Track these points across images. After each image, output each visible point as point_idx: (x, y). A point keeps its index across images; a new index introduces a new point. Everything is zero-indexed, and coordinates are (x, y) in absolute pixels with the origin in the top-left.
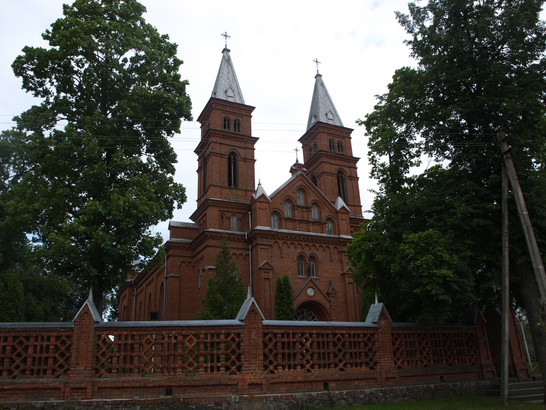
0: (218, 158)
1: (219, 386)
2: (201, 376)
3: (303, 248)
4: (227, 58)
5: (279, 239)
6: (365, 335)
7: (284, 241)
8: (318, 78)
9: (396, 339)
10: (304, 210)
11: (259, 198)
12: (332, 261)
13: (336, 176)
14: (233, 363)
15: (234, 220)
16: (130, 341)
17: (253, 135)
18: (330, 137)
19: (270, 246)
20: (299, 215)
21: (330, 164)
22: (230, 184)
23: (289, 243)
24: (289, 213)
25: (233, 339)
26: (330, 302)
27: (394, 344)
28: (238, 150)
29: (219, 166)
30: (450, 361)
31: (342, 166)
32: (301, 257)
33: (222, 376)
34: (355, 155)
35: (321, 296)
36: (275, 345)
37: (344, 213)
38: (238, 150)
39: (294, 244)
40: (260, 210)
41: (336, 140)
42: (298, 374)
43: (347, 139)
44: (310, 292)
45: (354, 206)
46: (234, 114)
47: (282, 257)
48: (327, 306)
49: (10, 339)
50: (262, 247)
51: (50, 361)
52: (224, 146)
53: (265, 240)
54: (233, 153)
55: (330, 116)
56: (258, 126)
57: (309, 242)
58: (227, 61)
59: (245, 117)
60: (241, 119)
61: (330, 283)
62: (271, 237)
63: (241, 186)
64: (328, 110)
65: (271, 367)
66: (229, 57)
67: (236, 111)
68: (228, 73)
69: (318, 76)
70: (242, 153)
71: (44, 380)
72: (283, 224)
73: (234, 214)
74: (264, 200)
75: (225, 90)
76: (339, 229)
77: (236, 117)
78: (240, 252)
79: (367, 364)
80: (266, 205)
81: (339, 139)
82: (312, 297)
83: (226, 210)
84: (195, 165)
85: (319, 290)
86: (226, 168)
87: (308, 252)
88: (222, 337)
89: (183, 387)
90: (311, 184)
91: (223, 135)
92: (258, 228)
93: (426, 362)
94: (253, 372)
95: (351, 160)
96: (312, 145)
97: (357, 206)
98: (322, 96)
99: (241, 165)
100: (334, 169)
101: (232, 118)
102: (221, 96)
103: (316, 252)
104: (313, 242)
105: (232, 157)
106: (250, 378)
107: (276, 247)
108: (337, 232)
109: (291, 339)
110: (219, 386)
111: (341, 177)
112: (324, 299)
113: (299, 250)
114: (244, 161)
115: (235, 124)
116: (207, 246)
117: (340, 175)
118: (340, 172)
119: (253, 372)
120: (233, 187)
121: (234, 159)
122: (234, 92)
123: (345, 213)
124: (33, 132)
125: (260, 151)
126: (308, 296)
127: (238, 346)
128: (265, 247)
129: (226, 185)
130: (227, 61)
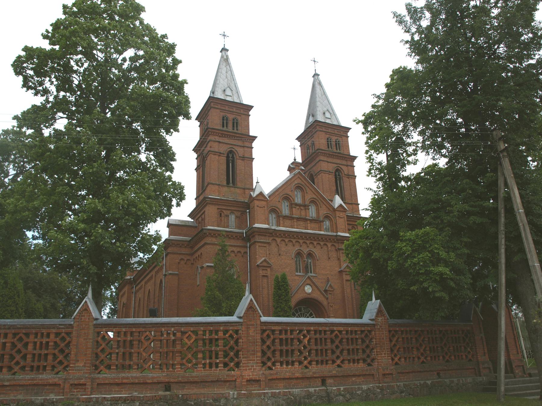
0: (217, 157)
1: (217, 382)
2: (200, 373)
3: (301, 246)
4: (225, 57)
5: (277, 237)
6: (362, 332)
7: (282, 239)
8: (316, 77)
9: (393, 336)
10: (302, 208)
11: (258, 196)
12: (329, 258)
13: (334, 174)
14: (232, 360)
15: (232, 218)
16: (129, 338)
17: (251, 134)
18: (327, 136)
19: (268, 243)
20: (296, 213)
21: (328, 162)
22: (228, 183)
23: (287, 240)
24: (287, 211)
25: (231, 336)
26: (327, 299)
27: (391, 341)
28: (236, 148)
29: (217, 165)
30: (447, 357)
31: (340, 164)
32: (299, 254)
33: (220, 372)
34: (352, 153)
35: (319, 293)
36: (273, 341)
37: (341, 211)
38: (236, 148)
39: (291, 241)
40: (258, 208)
41: (334, 138)
42: (296, 370)
43: (344, 138)
44: (308, 289)
45: (352, 204)
46: (232, 112)
47: (280, 255)
48: (325, 303)
49: (10, 336)
50: (260, 244)
51: (50, 358)
52: (222, 144)
53: (263, 237)
54: (231, 152)
55: (327, 115)
56: (256, 125)
57: (307, 239)
58: (225, 60)
59: (243, 116)
60: (239, 118)
61: (328, 280)
62: (269, 235)
63: (239, 184)
64: (325, 109)
65: (269, 364)
66: (227, 56)
67: (234, 110)
68: (227, 72)
69: (316, 75)
70: (240, 151)
71: (44, 376)
72: (281, 222)
73: (232, 212)
74: (262, 198)
75: (223, 89)
76: (337, 227)
77: (234, 116)
78: (239, 249)
79: (364, 361)
80: (264, 203)
81: (336, 138)
82: (309, 294)
83: (224, 208)
84: (194, 164)
85: (317, 287)
86: (224, 167)
87: (305, 250)
88: (221, 334)
89: (182, 384)
90: (309, 183)
91: (222, 134)
92: (257, 225)
93: (422, 359)
94: (252, 368)
95: (348, 158)
96: (309, 143)
97: (354, 204)
98: (320, 95)
99: (240, 164)
100: (331, 167)
101: (231, 117)
102: (219, 95)
103: (314, 250)
104: (311, 240)
105: (231, 156)
106: (248, 374)
107: (274, 244)
108: (335, 230)
109: (289, 336)
110: (217, 382)
111: (339, 175)
112: (322, 295)
113: (297, 248)
114: (242, 160)
115: (233, 123)
116: (206, 244)
117: (337, 174)
118: (337, 170)
119: (252, 368)
120: (231, 185)
121: (233, 157)
122: (232, 91)
123: (343, 211)
124: (33, 131)
125: (258, 150)
126: (306, 293)
127: (237, 342)
128: (263, 245)
129: (225, 183)
130: (225, 60)
